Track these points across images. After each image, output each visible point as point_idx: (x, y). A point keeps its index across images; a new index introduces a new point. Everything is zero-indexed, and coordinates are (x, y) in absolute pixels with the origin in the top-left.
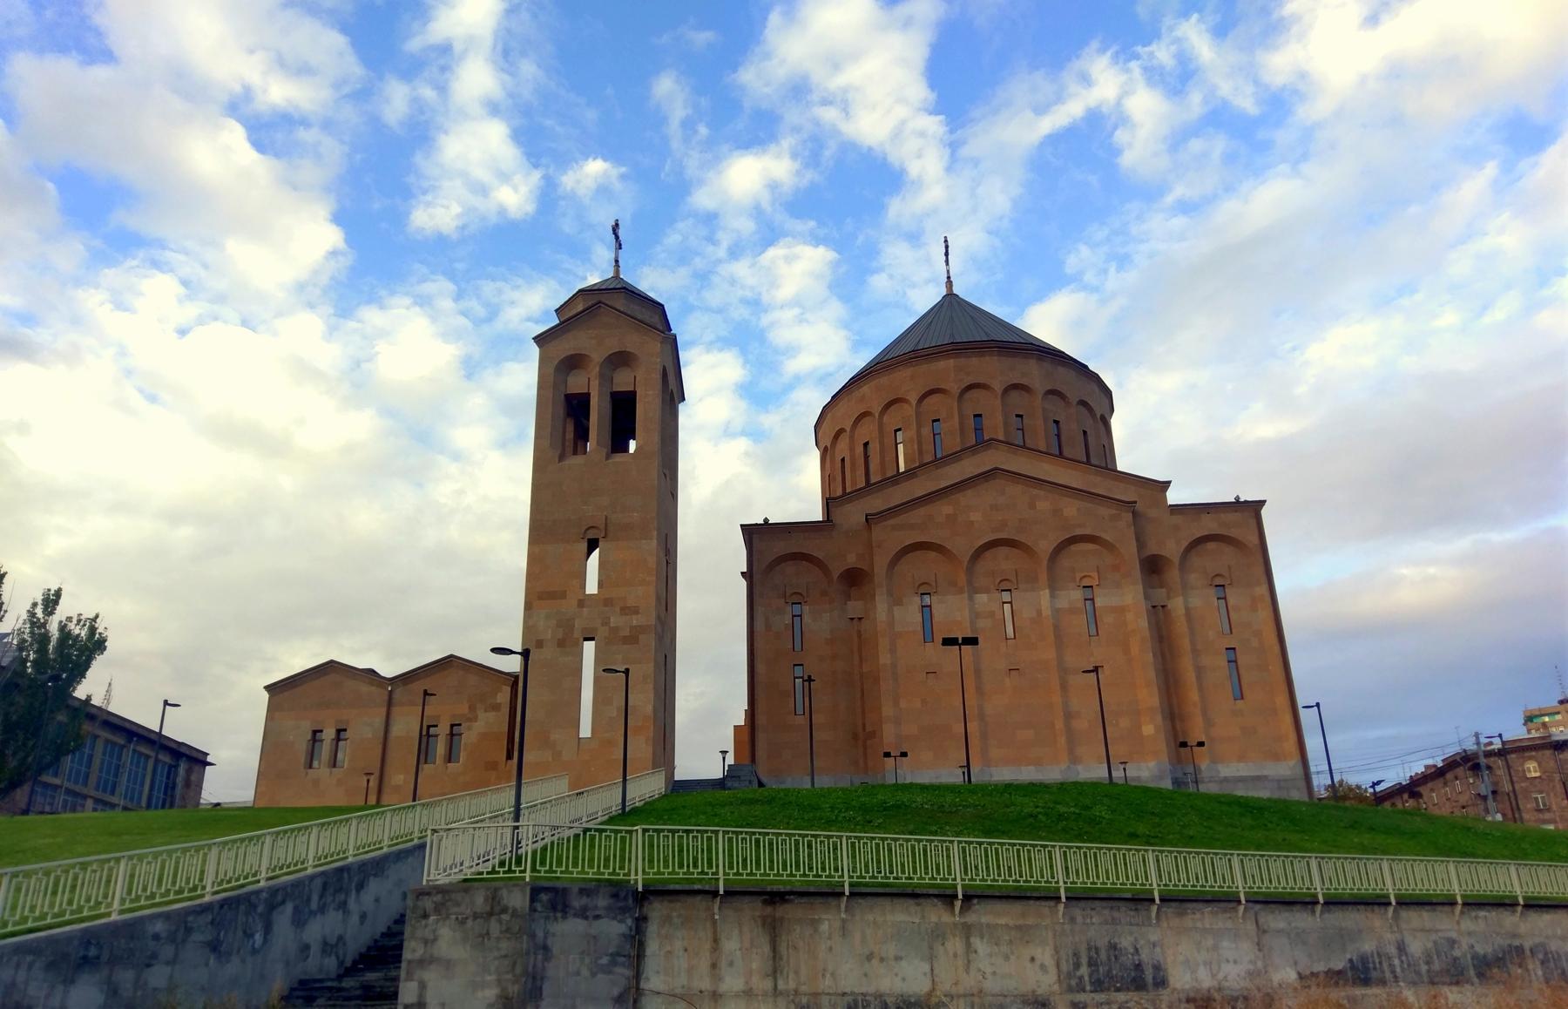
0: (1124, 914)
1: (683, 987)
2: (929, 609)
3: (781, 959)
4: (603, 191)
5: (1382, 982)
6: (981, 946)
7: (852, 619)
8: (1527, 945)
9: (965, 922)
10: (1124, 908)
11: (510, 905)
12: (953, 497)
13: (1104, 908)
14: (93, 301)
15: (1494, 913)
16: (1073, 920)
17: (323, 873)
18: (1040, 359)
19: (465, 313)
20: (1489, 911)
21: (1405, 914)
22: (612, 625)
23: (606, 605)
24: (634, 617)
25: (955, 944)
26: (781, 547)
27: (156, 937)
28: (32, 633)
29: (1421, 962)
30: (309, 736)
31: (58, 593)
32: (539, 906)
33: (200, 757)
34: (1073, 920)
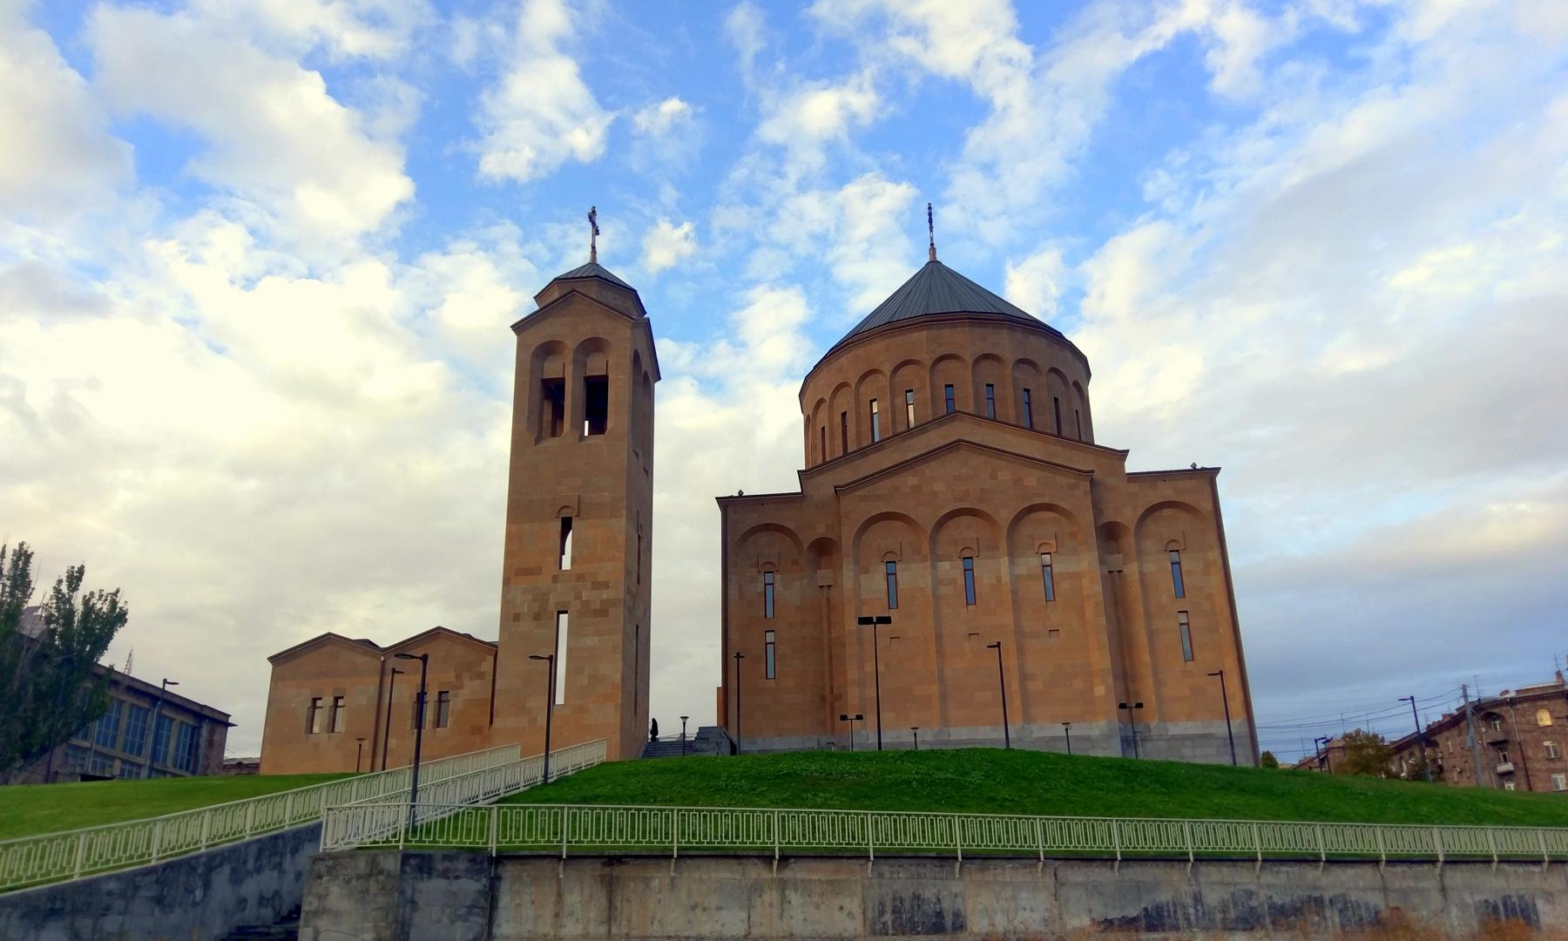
0: (929, 870)
1: (530, 932)
2: (894, 576)
3: (616, 909)
4: (676, 129)
5: (1176, 928)
6: (794, 897)
7: (821, 587)
8: (1327, 896)
9: (782, 878)
10: (929, 866)
11: (386, 867)
12: (918, 468)
13: (910, 865)
14: (166, 252)
15: (1297, 868)
16: (881, 875)
17: (258, 840)
18: (1011, 328)
19: (529, 258)
20: (1290, 867)
21: (1203, 868)
24: (605, 591)
25: (772, 896)
26: (752, 519)
27: (110, 894)
28: (58, 608)
29: (1217, 911)
30: (309, 703)
31: (81, 570)
32: (408, 869)
33: (223, 718)
34: (881, 875)
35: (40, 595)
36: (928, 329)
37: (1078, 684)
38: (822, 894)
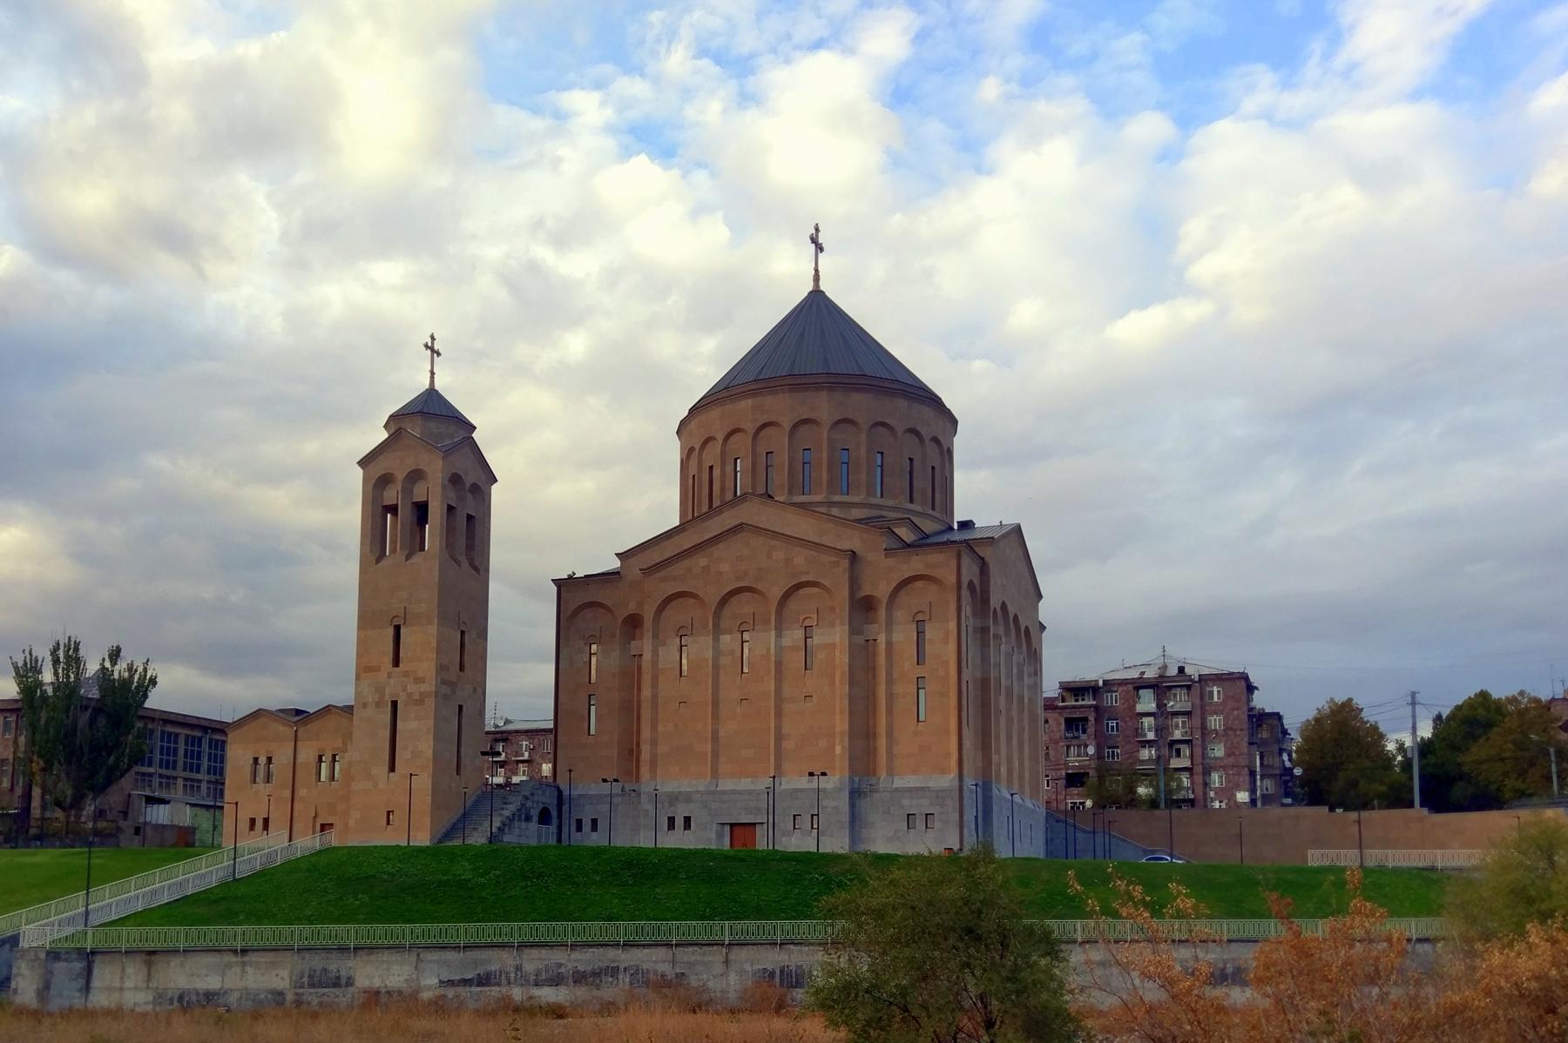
0: (334, 955)
6: (249, 970)
8: (622, 966)
23: (404, 676)
26: (580, 598)
35: (92, 668)
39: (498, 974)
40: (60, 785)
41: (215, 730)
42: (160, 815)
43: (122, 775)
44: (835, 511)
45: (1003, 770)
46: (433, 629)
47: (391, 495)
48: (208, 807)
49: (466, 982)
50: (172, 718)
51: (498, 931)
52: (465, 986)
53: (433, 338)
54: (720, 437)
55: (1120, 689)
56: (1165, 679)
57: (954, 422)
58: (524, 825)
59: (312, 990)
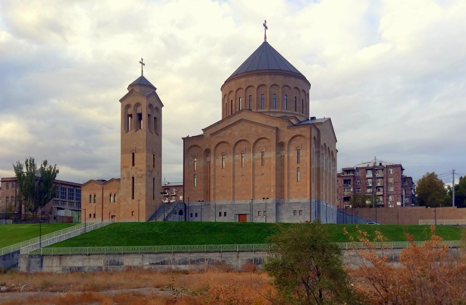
0: (117, 256)
5: (168, 264)
6: (91, 260)
12: (231, 128)
22: (137, 174)
23: (136, 169)
26: (191, 144)
35: (38, 167)
36: (245, 78)
37: (267, 189)
38: (96, 260)
39: (167, 261)
40: (30, 204)
41: (77, 187)
42: (62, 213)
43: (49, 201)
44: (271, 115)
45: (324, 196)
46: (145, 154)
47: (130, 111)
48: (76, 211)
49: (157, 264)
50: (64, 183)
51: (167, 248)
52: (157, 265)
53: (142, 60)
54: (235, 91)
55: (361, 170)
56: (376, 167)
57: (309, 85)
58: (174, 215)
59: (111, 266)
